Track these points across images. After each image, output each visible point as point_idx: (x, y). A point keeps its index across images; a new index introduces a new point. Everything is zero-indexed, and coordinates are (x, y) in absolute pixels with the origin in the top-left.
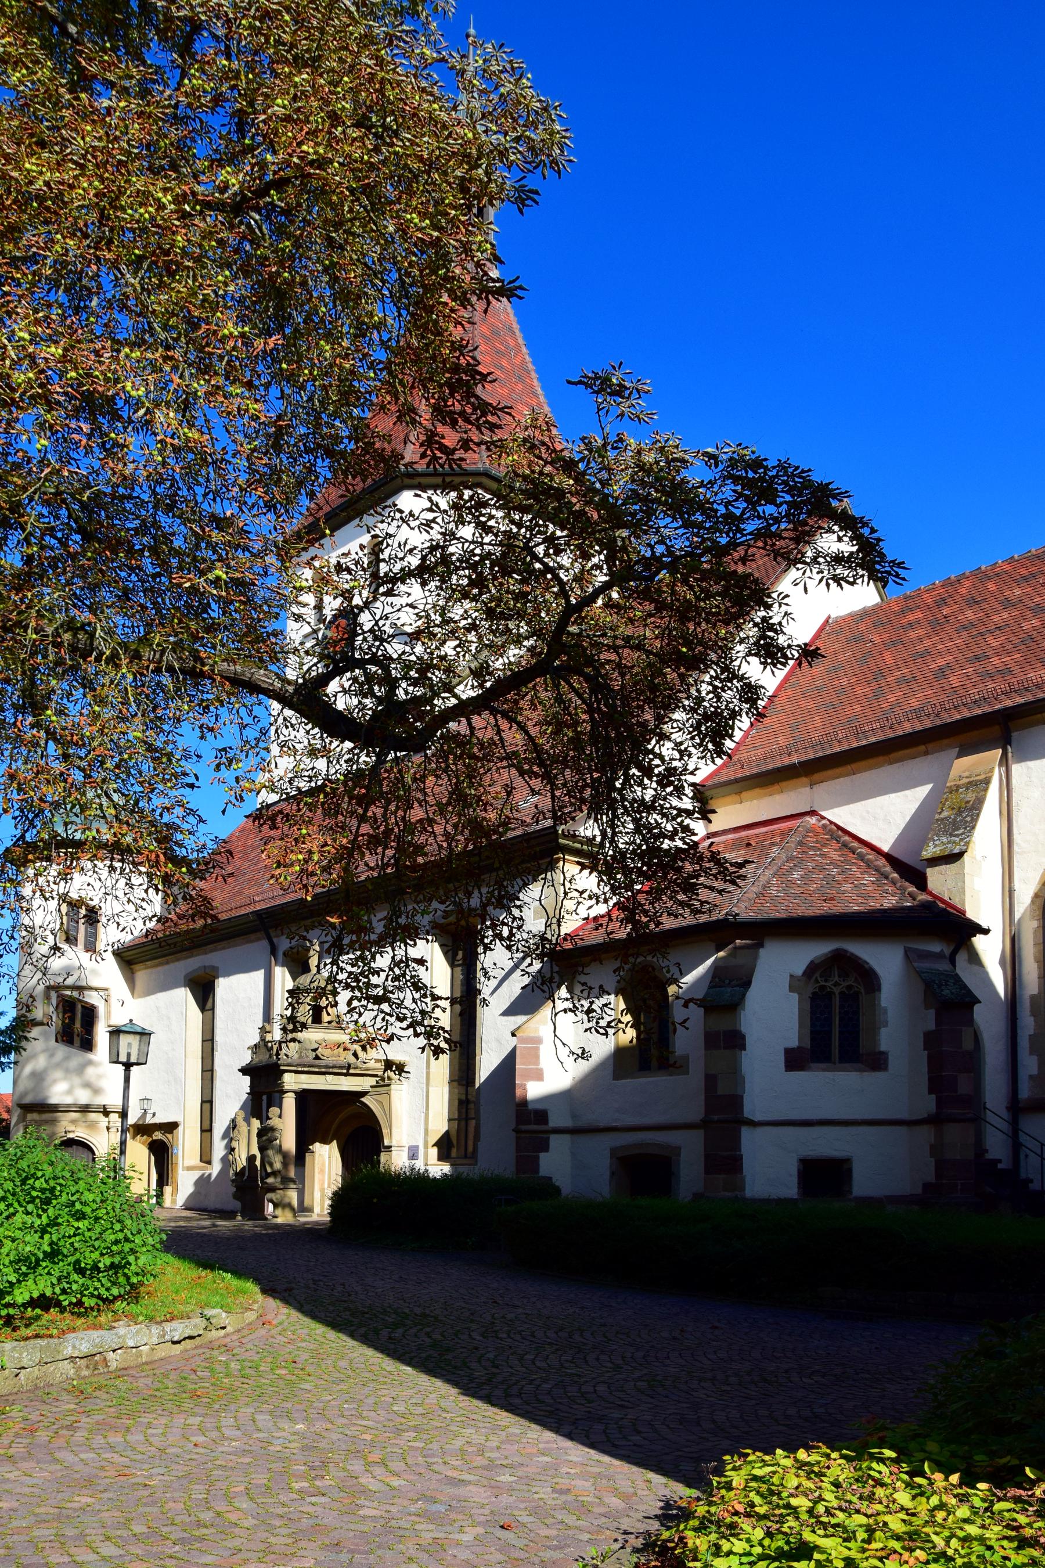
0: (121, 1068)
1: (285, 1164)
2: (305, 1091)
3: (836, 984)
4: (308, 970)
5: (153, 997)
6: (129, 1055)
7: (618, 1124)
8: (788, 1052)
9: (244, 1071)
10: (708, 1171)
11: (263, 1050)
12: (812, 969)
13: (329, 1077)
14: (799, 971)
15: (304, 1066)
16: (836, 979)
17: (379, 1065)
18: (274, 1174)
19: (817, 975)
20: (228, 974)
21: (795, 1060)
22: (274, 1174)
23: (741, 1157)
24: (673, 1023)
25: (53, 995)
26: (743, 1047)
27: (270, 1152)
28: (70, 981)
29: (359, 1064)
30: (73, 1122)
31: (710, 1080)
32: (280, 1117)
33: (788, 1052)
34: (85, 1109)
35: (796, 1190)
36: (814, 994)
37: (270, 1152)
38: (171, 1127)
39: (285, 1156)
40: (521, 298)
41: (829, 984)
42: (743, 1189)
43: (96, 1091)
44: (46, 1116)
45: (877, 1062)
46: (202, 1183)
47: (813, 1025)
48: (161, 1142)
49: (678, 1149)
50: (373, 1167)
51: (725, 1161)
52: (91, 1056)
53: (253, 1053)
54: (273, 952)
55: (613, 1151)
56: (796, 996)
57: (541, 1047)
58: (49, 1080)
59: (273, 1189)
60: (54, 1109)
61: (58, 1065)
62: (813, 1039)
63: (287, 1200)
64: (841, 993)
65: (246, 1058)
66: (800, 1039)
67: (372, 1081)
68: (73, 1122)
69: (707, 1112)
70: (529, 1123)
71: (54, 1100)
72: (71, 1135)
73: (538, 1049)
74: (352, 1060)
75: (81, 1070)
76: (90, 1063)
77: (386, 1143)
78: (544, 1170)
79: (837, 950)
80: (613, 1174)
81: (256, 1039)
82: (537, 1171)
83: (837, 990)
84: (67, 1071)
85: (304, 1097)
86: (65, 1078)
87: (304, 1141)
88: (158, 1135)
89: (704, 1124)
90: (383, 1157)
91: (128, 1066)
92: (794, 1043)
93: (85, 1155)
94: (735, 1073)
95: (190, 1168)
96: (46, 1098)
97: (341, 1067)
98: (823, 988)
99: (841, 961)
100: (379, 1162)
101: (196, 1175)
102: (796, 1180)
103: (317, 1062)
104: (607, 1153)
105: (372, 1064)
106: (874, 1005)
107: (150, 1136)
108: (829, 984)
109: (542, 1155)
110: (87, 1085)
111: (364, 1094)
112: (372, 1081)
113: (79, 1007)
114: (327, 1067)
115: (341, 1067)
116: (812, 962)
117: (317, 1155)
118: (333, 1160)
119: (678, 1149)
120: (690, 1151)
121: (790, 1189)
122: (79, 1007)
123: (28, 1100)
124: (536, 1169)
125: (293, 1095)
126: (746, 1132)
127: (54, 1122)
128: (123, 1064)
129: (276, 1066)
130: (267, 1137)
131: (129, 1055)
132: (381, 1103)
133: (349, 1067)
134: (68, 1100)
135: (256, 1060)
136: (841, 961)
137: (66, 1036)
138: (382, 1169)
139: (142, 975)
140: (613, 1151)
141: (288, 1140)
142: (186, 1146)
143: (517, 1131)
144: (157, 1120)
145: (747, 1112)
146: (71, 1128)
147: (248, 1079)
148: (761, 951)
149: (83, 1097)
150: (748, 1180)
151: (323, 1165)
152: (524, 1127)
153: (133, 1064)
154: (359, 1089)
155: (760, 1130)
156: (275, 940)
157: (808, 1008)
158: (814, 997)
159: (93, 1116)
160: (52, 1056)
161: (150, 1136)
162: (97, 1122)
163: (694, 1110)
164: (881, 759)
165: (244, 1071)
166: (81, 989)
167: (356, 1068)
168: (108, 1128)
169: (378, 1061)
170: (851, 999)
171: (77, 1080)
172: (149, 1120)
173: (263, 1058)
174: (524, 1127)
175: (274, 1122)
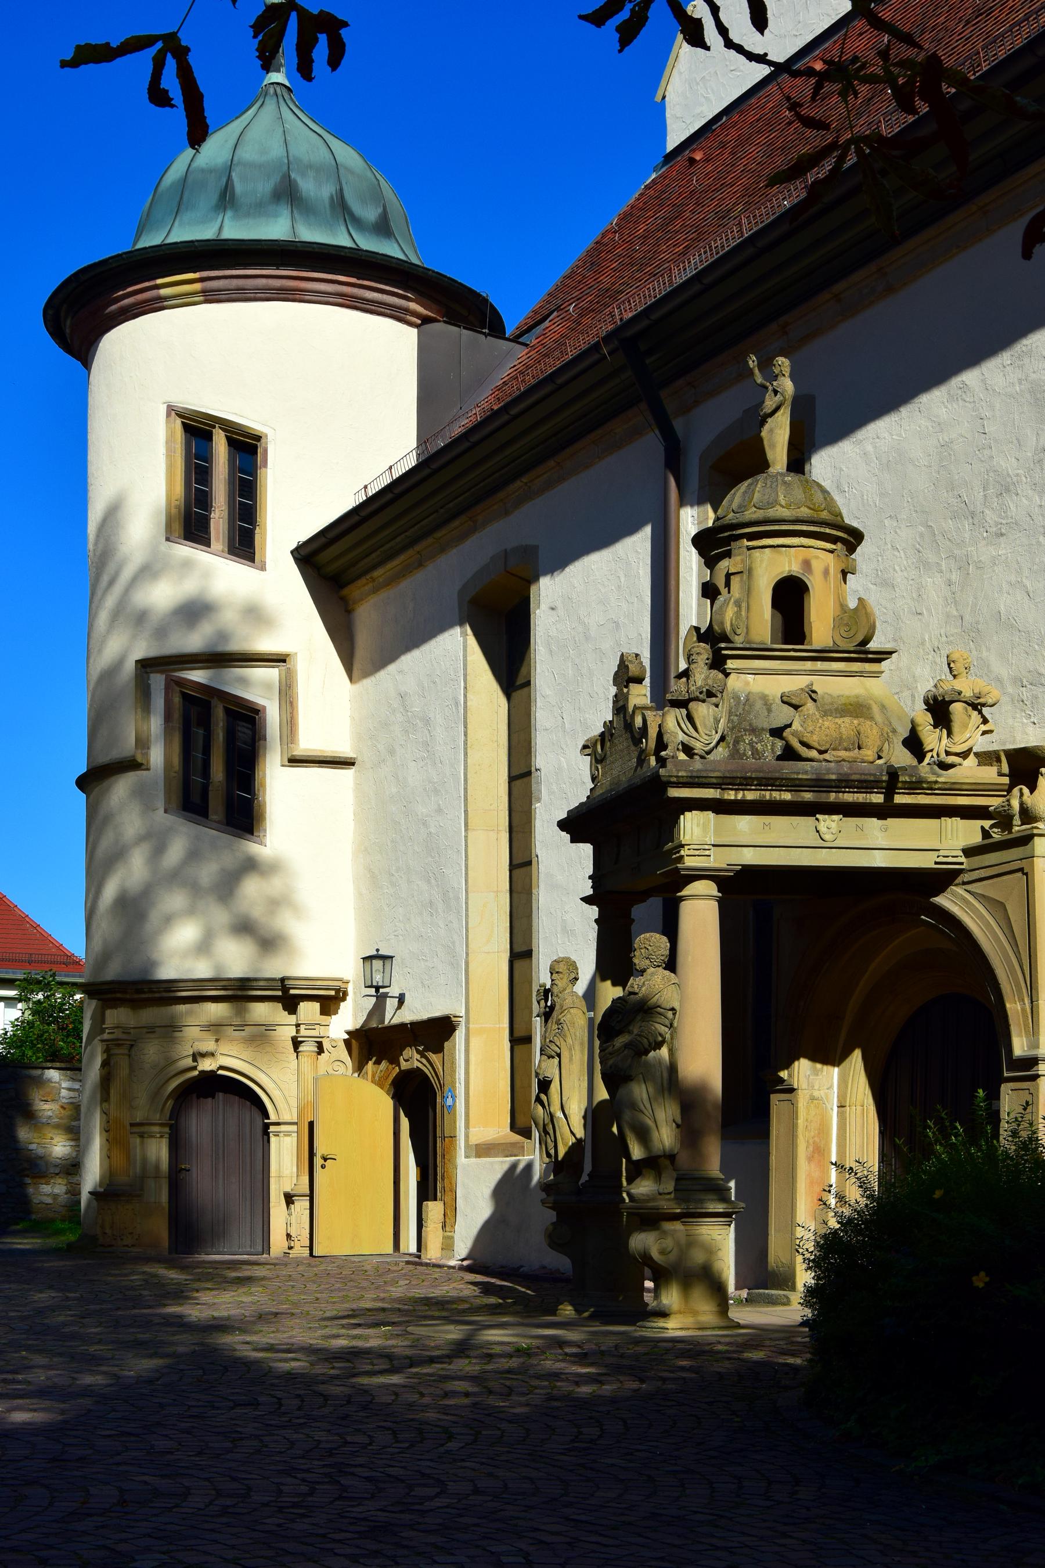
1: (690, 1130)
2: (749, 872)
4: (761, 465)
5: (392, 668)
11: (622, 742)
13: (829, 823)
15: (744, 783)
17: (989, 774)
18: (653, 1164)
20: (559, 563)
22: (653, 1164)
25: (157, 681)
27: (640, 1091)
28: (194, 641)
29: (925, 769)
30: (215, 1028)
32: (671, 964)
34: (239, 992)
37: (640, 1091)
38: (437, 1032)
39: (688, 1099)
43: (269, 942)
44: (149, 1015)
46: (510, 1188)
48: (416, 1074)
50: (974, 1134)
52: (253, 848)
53: (598, 760)
54: (674, 460)
58: (154, 917)
59: (650, 1219)
60: (167, 994)
61: (175, 877)
63: (698, 1257)
67: (966, 833)
68: (215, 1028)
71: (167, 972)
72: (207, 1065)
74: (902, 757)
75: (227, 886)
76: (251, 865)
77: (1020, 1047)
84: (195, 890)
85: (747, 892)
86: (191, 911)
87: (761, 1045)
88: (411, 1059)
90: (1009, 1100)
93: (250, 1114)
95: (483, 1150)
96: (153, 964)
97: (866, 785)
100: (994, 1117)
101: (496, 1167)
103: (789, 768)
105: (969, 771)
107: (394, 1061)
110: (244, 927)
111: (942, 878)
112: (966, 833)
113: (219, 714)
114: (819, 784)
115: (866, 785)
117: (802, 1099)
118: (853, 1113)
122: (219, 714)
123: (113, 972)
125: (706, 888)
127: (171, 1030)
129: (657, 785)
130: (627, 1035)
132: (998, 907)
133: (892, 780)
134: (202, 969)
135: (606, 782)
137: (191, 799)
138: (1005, 1141)
139: (295, 553)
141: (700, 1050)
142: (478, 1080)
144: (408, 1015)
146: (209, 1045)
147: (586, 850)
149: (235, 959)
151: (823, 1130)
154: (926, 861)
156: (678, 425)
159: (261, 1011)
160: (159, 850)
161: (394, 1061)
162: (270, 1027)
166: (220, 659)
167: (916, 786)
168: (296, 1043)
169: (987, 758)
171: (220, 916)
172: (393, 1016)
173: (623, 769)
175: (654, 983)
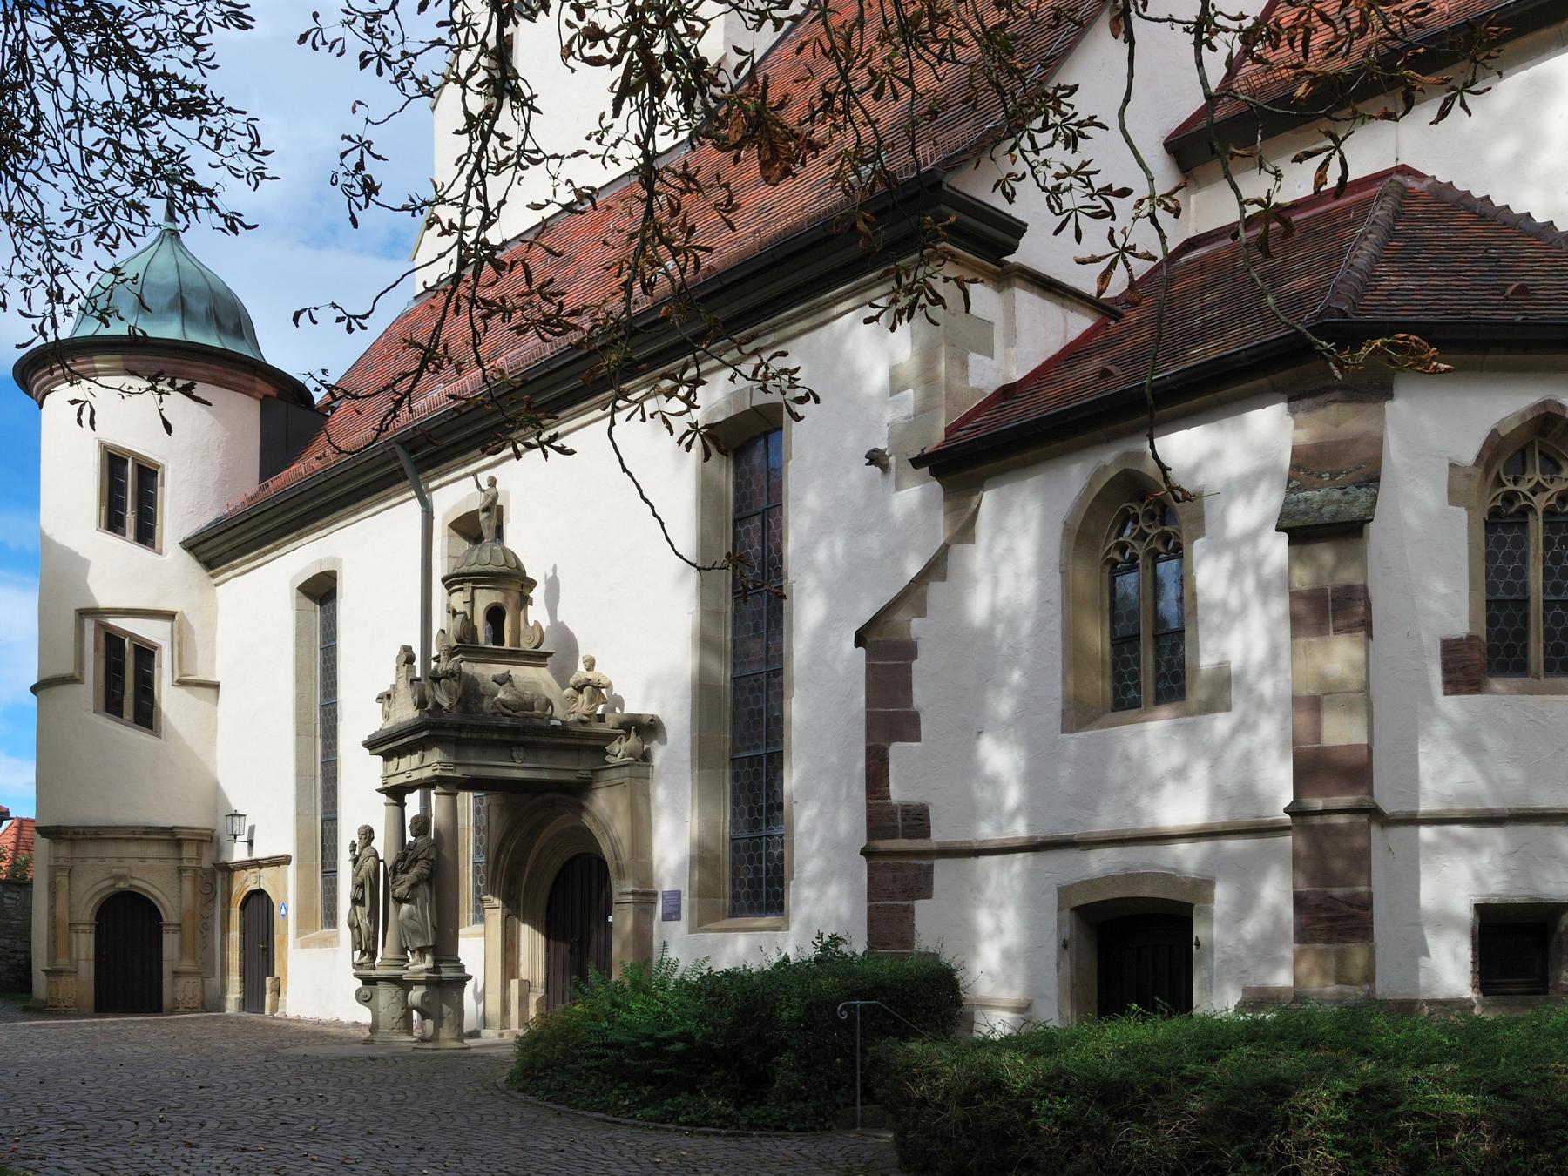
14: (1468, 452)
16: (1538, 476)
19: (1499, 466)
21: (1466, 668)
24: (645, 899)
33: (1451, 649)
36: (1494, 513)
40: (546, 456)
41: (1523, 488)
47: (1491, 587)
51: (1335, 915)
55: (1064, 892)
57: (916, 665)
62: (1491, 620)
64: (1549, 512)
70: (894, 837)
73: (908, 670)
79: (1544, 404)
80: (1065, 945)
92: (1460, 626)
98: (1510, 498)
108: (1523, 488)
109: (919, 905)
114: (514, 730)
116: (1494, 432)
124: (907, 940)
140: (1064, 892)
152: (883, 845)
165: (380, 791)
174: (883, 845)
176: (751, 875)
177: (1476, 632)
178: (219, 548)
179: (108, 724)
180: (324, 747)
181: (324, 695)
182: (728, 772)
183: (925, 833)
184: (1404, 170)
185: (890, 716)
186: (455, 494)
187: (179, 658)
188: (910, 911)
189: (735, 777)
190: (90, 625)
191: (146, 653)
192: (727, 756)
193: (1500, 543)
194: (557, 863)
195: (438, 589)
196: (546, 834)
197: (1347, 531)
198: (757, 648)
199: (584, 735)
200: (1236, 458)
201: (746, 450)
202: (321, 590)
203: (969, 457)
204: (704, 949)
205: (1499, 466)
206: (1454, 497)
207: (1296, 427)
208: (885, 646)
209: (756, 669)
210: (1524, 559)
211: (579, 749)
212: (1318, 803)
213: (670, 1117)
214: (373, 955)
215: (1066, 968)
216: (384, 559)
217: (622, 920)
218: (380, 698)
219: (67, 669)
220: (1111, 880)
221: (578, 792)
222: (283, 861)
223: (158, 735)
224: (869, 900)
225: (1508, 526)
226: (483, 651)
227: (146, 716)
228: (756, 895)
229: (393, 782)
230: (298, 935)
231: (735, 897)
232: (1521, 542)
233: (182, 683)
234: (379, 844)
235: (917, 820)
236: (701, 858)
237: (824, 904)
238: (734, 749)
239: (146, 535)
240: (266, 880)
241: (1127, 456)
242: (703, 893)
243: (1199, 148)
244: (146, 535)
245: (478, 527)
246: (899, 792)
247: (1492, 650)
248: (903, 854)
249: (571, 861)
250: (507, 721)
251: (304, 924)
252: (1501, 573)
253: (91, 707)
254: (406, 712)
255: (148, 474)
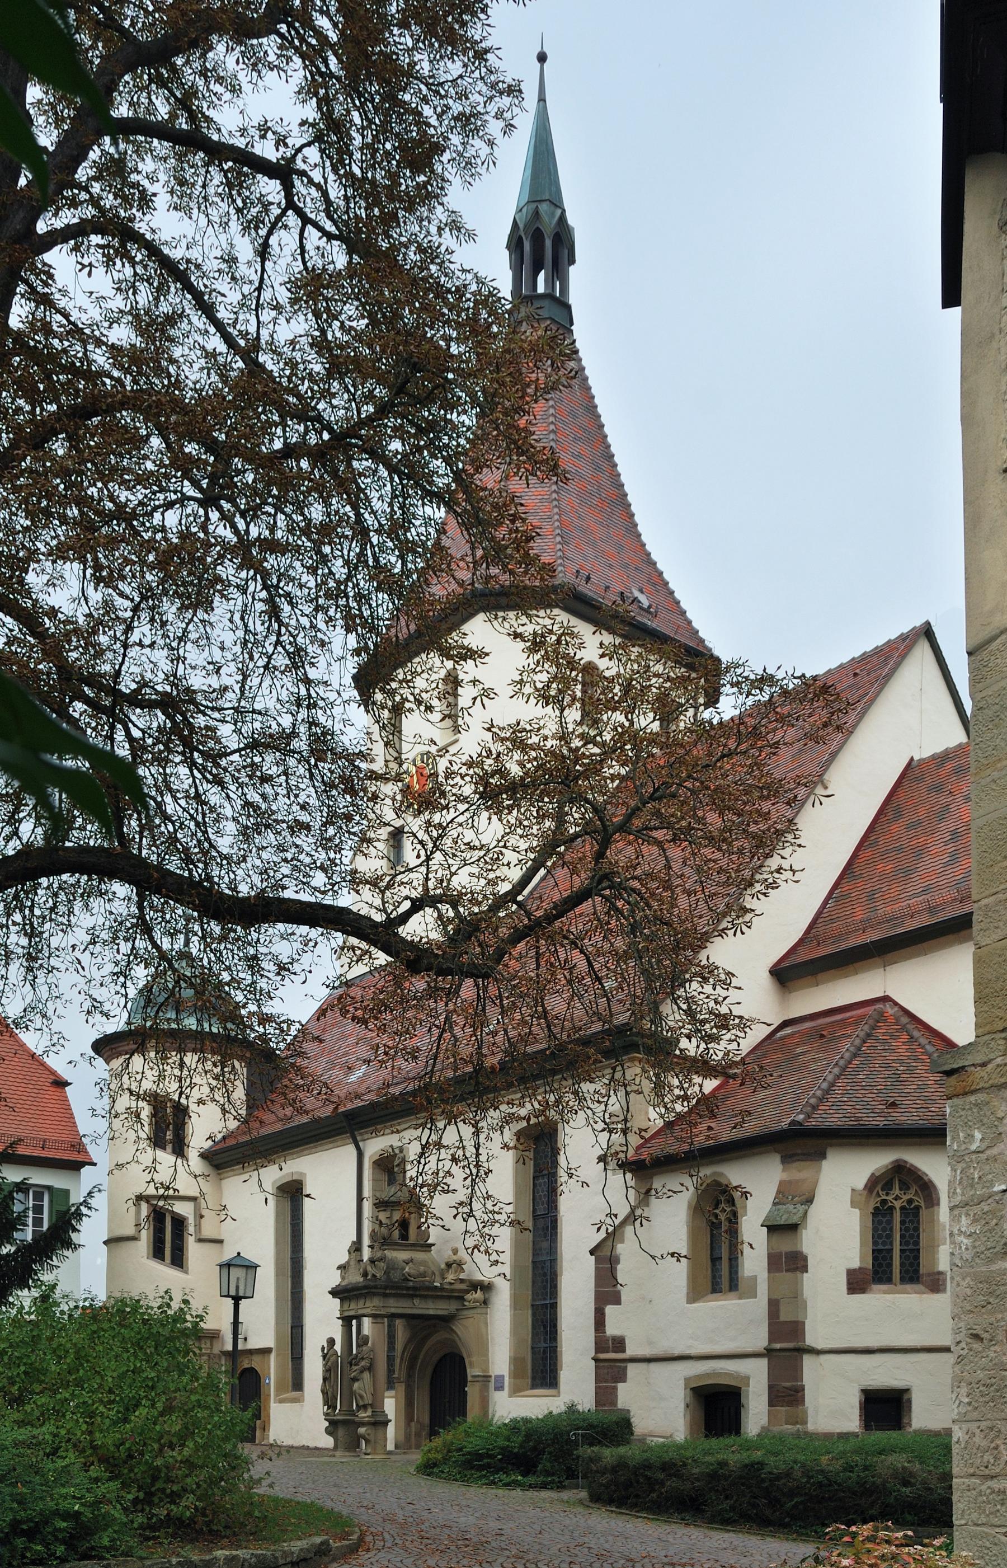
0: (230, 1302)
3: (898, 1198)
6: (237, 1288)
7: (693, 1352)
8: (850, 1273)
9: (335, 1293)
10: (771, 1403)
12: (874, 1183)
13: (416, 1301)
14: (860, 1183)
19: (879, 1188)
23: (802, 1388)
26: (805, 1269)
31: (774, 1306)
33: (850, 1273)
35: (857, 1423)
36: (876, 1209)
41: (890, 1198)
42: (805, 1422)
45: (935, 1284)
47: (875, 1243)
49: (747, 1379)
51: (787, 1394)
55: (687, 1380)
56: (857, 1211)
62: (874, 1259)
64: (902, 1208)
65: (335, 1279)
66: (862, 1259)
69: (770, 1341)
78: (622, 1402)
80: (687, 1406)
81: (344, 1258)
82: (616, 1405)
83: (898, 1204)
89: (769, 1353)
91: (237, 1299)
92: (856, 1264)
94: (796, 1297)
98: (884, 1202)
99: (901, 1175)
102: (857, 1412)
104: (682, 1383)
106: (933, 1221)
108: (890, 1198)
109: (620, 1386)
114: (415, 1289)
119: (747, 1379)
120: (756, 1379)
121: (851, 1421)
124: (614, 1403)
126: (807, 1360)
128: (233, 1298)
131: (237, 1288)
136: (901, 1175)
140: (687, 1380)
143: (596, 1360)
145: (811, 1339)
148: (824, 1163)
150: (810, 1412)
152: (602, 1356)
153: (241, 1298)
155: (823, 1358)
157: (870, 1225)
158: (876, 1212)
163: (759, 1338)
164: (951, 937)
170: (912, 1215)
174: (602, 1356)
176: (542, 1368)
177: (864, 1266)
178: (222, 1159)
179: (155, 1266)
180: (293, 1283)
181: (293, 1252)
182: (530, 1312)
183: (624, 1351)
184: (886, 999)
185: (607, 1290)
186: (375, 1146)
187: (198, 1226)
188: (615, 1388)
189: (534, 1315)
190: (144, 1207)
191: (179, 1223)
192: (529, 1303)
193: (880, 1223)
194: (435, 1359)
195: (367, 1206)
196: (429, 1343)
197: (793, 1228)
198: (545, 1245)
199: (452, 1291)
200: (759, 1184)
201: (540, 1147)
202: (292, 1193)
203: (645, 1168)
204: (512, 1406)
205: (879, 1188)
206: (853, 1205)
207: (783, 1171)
208: (605, 1258)
209: (544, 1258)
210: (891, 1229)
211: (449, 1298)
212: (778, 1346)
213: (493, 1483)
214: (335, 1408)
215: (688, 1417)
216: (334, 1182)
217: (472, 1391)
218: (339, 1268)
219: (130, 1231)
220: (707, 1375)
221: (447, 1320)
222: (267, 1351)
223: (186, 1273)
224: (597, 1381)
225: (884, 1215)
226: (396, 1244)
227: (178, 1261)
228: (544, 1378)
229: (346, 1314)
230: (276, 1395)
231: (534, 1378)
232: (890, 1222)
233: (200, 1240)
234: (338, 1347)
235: (619, 1344)
236: (516, 1362)
237: (576, 1387)
238: (533, 1300)
239: (179, 1149)
240: (256, 1363)
241: (714, 1173)
242: (969, 938)
243: (787, 974)
244: (179, 1149)
245: (389, 1166)
246: (612, 1329)
247: (875, 1272)
248: (611, 1361)
249: (445, 1356)
250: (411, 1284)
251: (279, 1390)
252: (880, 1237)
253: (145, 1254)
254: (355, 1278)
255: (181, 1113)
